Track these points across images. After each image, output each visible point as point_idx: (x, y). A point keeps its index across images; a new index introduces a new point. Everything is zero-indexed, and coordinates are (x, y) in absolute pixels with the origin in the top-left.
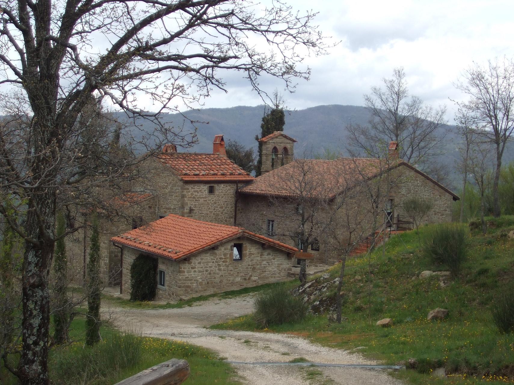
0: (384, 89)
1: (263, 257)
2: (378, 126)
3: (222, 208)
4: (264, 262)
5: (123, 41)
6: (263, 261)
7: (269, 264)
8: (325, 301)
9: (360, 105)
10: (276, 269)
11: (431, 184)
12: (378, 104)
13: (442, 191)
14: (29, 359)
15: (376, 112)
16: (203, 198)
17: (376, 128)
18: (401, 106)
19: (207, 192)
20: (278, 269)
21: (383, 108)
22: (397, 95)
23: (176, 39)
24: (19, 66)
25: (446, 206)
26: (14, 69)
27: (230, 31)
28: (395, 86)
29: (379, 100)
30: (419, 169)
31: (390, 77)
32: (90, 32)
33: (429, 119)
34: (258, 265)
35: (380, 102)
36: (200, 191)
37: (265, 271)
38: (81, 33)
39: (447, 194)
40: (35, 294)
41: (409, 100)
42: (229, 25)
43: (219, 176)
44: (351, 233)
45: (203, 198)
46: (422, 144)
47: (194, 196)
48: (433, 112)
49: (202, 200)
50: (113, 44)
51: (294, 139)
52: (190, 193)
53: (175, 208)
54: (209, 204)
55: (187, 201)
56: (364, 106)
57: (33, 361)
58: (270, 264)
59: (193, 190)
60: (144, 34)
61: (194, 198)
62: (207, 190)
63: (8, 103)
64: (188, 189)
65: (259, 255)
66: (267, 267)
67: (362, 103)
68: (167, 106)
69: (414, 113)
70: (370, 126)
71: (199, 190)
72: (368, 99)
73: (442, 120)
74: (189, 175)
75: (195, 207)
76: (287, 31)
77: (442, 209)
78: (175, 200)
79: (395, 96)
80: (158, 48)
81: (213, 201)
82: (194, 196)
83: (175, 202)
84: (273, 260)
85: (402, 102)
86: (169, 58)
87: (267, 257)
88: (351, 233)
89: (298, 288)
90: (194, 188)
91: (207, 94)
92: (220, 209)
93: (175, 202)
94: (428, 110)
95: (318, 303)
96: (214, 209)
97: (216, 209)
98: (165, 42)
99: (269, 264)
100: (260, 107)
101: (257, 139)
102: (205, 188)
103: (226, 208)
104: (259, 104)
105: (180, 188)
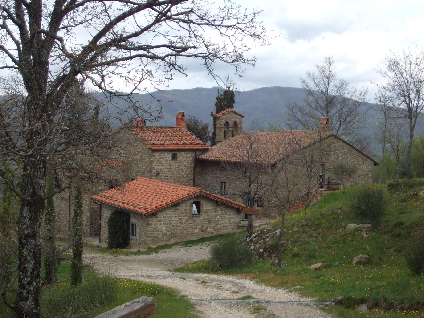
0: (317, 73)
1: (217, 212)
2: (312, 104)
4: (218, 217)
5: (102, 34)
6: (217, 215)
7: (222, 218)
8: (268, 248)
10: (227, 222)
11: (355, 152)
12: (312, 86)
13: (365, 158)
14: (24, 297)
15: (310, 93)
16: (168, 163)
17: (310, 106)
18: (330, 88)
19: (170, 158)
20: (229, 222)
21: (316, 89)
22: (327, 78)
23: (145, 32)
24: (16, 54)
28: (326, 71)
29: (313, 83)
30: (346, 140)
31: (322, 63)
32: (74, 27)
34: (213, 219)
36: (165, 158)
37: (219, 224)
39: (369, 160)
41: (337, 83)
45: (168, 163)
46: (348, 119)
47: (160, 162)
48: (358, 93)
49: (166, 165)
50: (94, 36)
51: (243, 115)
52: (156, 160)
53: (144, 172)
54: (172, 169)
55: (154, 166)
56: (300, 87)
57: (27, 298)
58: (223, 218)
59: (159, 157)
60: (119, 28)
61: (160, 163)
62: (171, 157)
64: (155, 156)
65: (214, 211)
67: (298, 85)
70: (305, 104)
71: (164, 157)
73: (365, 99)
75: (161, 171)
76: (237, 25)
78: (144, 165)
79: (326, 80)
80: (131, 40)
82: (160, 162)
84: (225, 215)
85: (331, 84)
86: (139, 48)
87: (220, 212)
89: (246, 238)
90: (160, 156)
91: (170, 78)
92: (181, 173)
95: (262, 250)
96: (177, 173)
97: (178, 172)
98: (136, 34)
99: (222, 218)
101: (212, 114)
102: (169, 155)
103: (186, 172)
105: (148, 155)
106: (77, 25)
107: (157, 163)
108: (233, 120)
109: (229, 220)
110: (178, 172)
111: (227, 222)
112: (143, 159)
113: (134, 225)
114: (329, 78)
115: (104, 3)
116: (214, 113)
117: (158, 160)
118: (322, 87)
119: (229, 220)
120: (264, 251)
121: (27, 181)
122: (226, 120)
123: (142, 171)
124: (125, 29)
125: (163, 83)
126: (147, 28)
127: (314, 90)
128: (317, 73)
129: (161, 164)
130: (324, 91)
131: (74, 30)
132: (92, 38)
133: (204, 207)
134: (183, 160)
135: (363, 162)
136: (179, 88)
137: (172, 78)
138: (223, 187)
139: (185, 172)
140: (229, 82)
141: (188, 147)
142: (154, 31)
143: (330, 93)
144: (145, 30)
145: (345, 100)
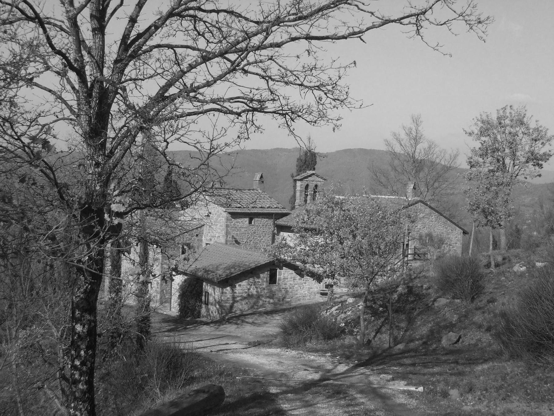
1: (295, 281)
3: (260, 237)
5: (170, 84)
7: (300, 288)
8: (350, 323)
9: (382, 149)
10: (306, 292)
11: (443, 219)
12: (398, 149)
13: (454, 226)
14: (76, 379)
15: (394, 155)
16: (244, 228)
17: (396, 170)
21: (402, 152)
22: (414, 140)
23: (218, 82)
24: (74, 104)
25: (457, 240)
26: (70, 108)
27: (268, 82)
28: (413, 133)
29: (398, 145)
31: (409, 124)
32: (143, 80)
33: (443, 163)
35: (399, 147)
37: (297, 294)
38: (135, 80)
40: (83, 318)
42: (268, 76)
43: (273, 209)
45: (244, 228)
46: (436, 184)
48: (447, 157)
49: (243, 230)
50: (161, 86)
52: (232, 224)
53: (219, 237)
54: (249, 233)
56: (385, 150)
57: (80, 381)
58: (302, 287)
60: (189, 79)
63: (74, 141)
67: (384, 148)
68: (137, 82)
69: (429, 157)
70: (390, 168)
72: (388, 144)
74: (264, 208)
75: (237, 236)
77: (453, 242)
78: (219, 229)
79: (413, 142)
80: (201, 91)
81: (252, 231)
83: (219, 231)
84: (304, 284)
86: (213, 101)
89: (325, 311)
91: (247, 137)
92: (258, 238)
95: (344, 324)
96: (254, 238)
97: (255, 238)
98: (208, 84)
99: (300, 288)
101: (293, 177)
102: (247, 220)
103: (264, 237)
105: (224, 219)
108: (315, 183)
109: (308, 290)
110: (255, 238)
111: (306, 292)
112: (218, 222)
113: (207, 293)
114: (416, 140)
115: (175, 51)
116: (295, 174)
117: (234, 224)
118: (410, 150)
119: (308, 290)
120: (345, 326)
121: (83, 248)
122: (307, 183)
123: (217, 236)
124: (196, 79)
125: (238, 143)
126: (220, 77)
127: (399, 153)
129: (237, 228)
130: (411, 154)
132: (159, 88)
134: (261, 225)
137: (249, 138)
139: (262, 237)
141: (265, 211)
143: (417, 155)
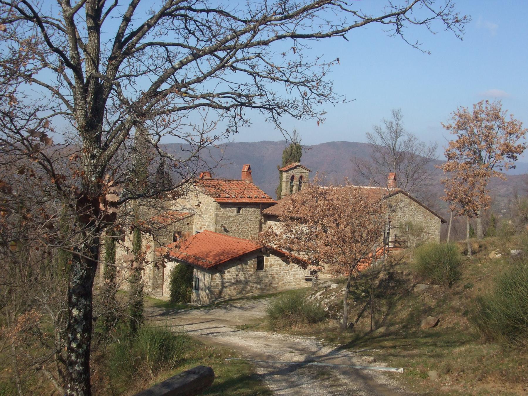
0: (384, 129)
2: (379, 160)
3: (248, 225)
5: (162, 80)
7: (286, 274)
8: (333, 307)
12: (379, 142)
13: (432, 215)
14: (73, 361)
15: (376, 147)
16: (233, 217)
17: (377, 162)
18: (398, 143)
21: (383, 145)
22: (395, 133)
23: (208, 78)
26: (67, 103)
28: (394, 127)
29: (379, 138)
30: (412, 195)
31: (390, 118)
33: (422, 155)
35: (381, 140)
37: (283, 280)
38: (129, 76)
39: (436, 217)
41: (405, 138)
44: (291, 72)
45: (233, 217)
46: (416, 176)
48: (426, 149)
49: (231, 219)
52: (221, 213)
53: (209, 225)
56: (367, 143)
57: (76, 363)
58: (288, 274)
60: (180, 75)
66: (284, 276)
67: (364, 140)
69: (409, 149)
73: (434, 155)
75: (226, 224)
79: (393, 135)
80: (192, 86)
81: (241, 220)
83: (209, 220)
84: (290, 271)
85: (400, 139)
86: (203, 96)
88: (291, 72)
89: (310, 296)
91: (235, 130)
92: (246, 227)
93: (209, 220)
94: (422, 147)
95: (328, 309)
97: (243, 226)
98: (199, 80)
99: (286, 274)
100: (282, 142)
102: (235, 209)
103: (251, 226)
104: (280, 140)
105: (213, 208)
106: (139, 75)
107: (222, 216)
108: (300, 174)
110: (243, 226)
111: (292, 278)
117: (223, 214)
118: (390, 143)
120: (329, 310)
122: (292, 174)
124: (186, 75)
125: (227, 136)
126: (210, 74)
127: (381, 146)
128: (384, 129)
129: (226, 217)
131: (137, 79)
133: (269, 262)
134: (249, 214)
135: (430, 219)
136: (246, 141)
137: (237, 131)
138: (323, 358)
139: (250, 226)
140: (296, 136)
141: (253, 201)
142: (218, 77)
143: (397, 148)
144: (223, 107)
145: (412, 155)
